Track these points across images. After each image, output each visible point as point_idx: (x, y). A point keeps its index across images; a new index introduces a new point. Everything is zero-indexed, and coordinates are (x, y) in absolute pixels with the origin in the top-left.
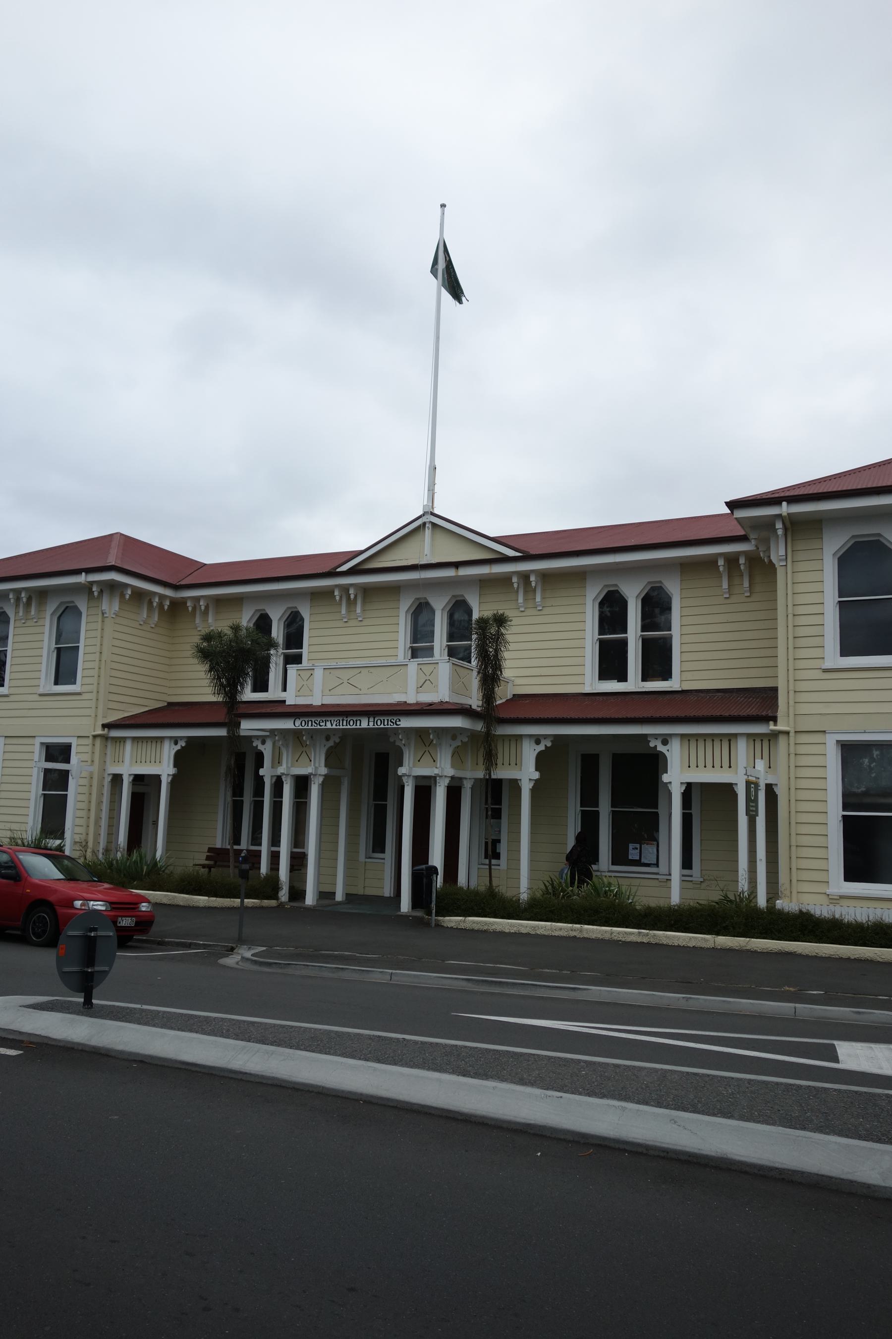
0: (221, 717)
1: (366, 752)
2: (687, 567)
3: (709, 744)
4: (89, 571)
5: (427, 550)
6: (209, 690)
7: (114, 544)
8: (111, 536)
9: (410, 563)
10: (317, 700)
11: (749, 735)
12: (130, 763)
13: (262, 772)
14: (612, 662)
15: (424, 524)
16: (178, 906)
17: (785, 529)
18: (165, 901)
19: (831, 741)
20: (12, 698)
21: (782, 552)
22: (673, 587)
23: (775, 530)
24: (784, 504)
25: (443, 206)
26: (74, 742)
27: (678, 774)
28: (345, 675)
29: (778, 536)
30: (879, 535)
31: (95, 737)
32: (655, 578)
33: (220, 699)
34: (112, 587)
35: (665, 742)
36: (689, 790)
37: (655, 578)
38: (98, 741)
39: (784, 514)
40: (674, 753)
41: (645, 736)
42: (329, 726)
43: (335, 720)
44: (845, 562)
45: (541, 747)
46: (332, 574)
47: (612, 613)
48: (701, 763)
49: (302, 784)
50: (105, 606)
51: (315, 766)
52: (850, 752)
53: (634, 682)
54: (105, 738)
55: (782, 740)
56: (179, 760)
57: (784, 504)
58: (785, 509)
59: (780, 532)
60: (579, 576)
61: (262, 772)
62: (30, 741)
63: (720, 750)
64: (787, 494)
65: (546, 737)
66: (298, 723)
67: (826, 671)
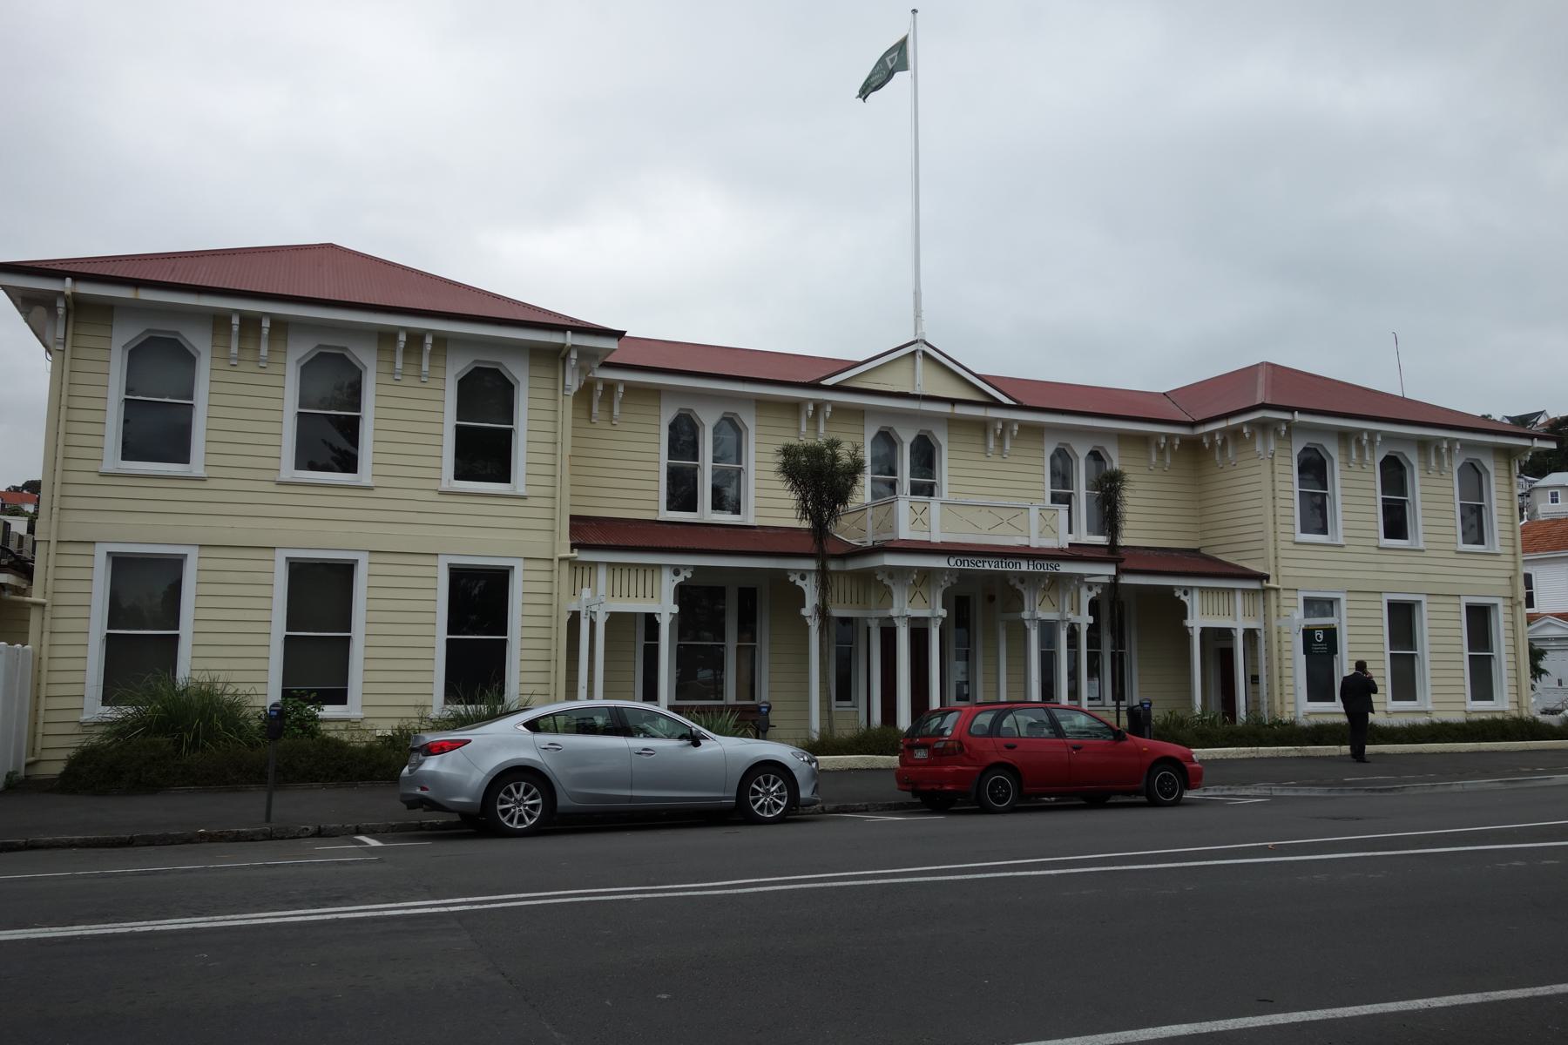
0: (809, 545)
1: (982, 595)
2: (762, 404)
3: (625, 573)
4: (1303, 411)
5: (925, 381)
6: (793, 513)
7: (1261, 379)
8: (1252, 371)
9: (896, 389)
10: (937, 537)
11: (609, 564)
12: (603, 597)
13: (1091, 620)
14: (682, 491)
15: (914, 353)
16: (879, 769)
17: (67, 310)
18: (862, 765)
19: (101, 552)
20: (210, 484)
21: (60, 334)
22: (942, 438)
23: (260, 328)
24: (68, 280)
25: (915, 11)
26: (1343, 597)
27: (1197, 621)
28: (1006, 514)
29: (56, 315)
30: (177, 333)
31: (561, 559)
32: (686, 405)
33: (806, 524)
34: (1264, 426)
35: (803, 578)
36: (1204, 631)
37: (686, 405)
38: (565, 567)
39: (68, 292)
40: (1194, 603)
41: (785, 571)
42: (987, 567)
43: (993, 561)
44: (136, 354)
45: (680, 579)
46: (815, 386)
47: (683, 439)
48: (633, 594)
49: (1048, 631)
50: (1259, 448)
51: (935, 610)
52: (120, 563)
53: (705, 513)
54: (573, 564)
55: (1273, 595)
56: (683, 594)
57: (68, 280)
58: (68, 286)
59: (266, 332)
60: (654, 394)
61: (1091, 620)
62: (1377, 597)
63: (1222, 600)
64: (72, 268)
65: (685, 567)
66: (952, 562)
67: (442, 493)
